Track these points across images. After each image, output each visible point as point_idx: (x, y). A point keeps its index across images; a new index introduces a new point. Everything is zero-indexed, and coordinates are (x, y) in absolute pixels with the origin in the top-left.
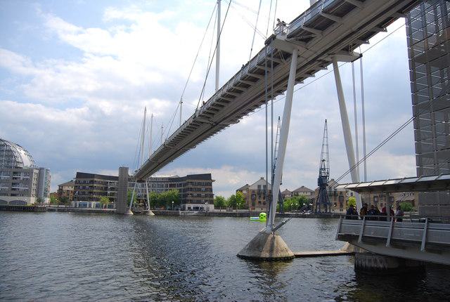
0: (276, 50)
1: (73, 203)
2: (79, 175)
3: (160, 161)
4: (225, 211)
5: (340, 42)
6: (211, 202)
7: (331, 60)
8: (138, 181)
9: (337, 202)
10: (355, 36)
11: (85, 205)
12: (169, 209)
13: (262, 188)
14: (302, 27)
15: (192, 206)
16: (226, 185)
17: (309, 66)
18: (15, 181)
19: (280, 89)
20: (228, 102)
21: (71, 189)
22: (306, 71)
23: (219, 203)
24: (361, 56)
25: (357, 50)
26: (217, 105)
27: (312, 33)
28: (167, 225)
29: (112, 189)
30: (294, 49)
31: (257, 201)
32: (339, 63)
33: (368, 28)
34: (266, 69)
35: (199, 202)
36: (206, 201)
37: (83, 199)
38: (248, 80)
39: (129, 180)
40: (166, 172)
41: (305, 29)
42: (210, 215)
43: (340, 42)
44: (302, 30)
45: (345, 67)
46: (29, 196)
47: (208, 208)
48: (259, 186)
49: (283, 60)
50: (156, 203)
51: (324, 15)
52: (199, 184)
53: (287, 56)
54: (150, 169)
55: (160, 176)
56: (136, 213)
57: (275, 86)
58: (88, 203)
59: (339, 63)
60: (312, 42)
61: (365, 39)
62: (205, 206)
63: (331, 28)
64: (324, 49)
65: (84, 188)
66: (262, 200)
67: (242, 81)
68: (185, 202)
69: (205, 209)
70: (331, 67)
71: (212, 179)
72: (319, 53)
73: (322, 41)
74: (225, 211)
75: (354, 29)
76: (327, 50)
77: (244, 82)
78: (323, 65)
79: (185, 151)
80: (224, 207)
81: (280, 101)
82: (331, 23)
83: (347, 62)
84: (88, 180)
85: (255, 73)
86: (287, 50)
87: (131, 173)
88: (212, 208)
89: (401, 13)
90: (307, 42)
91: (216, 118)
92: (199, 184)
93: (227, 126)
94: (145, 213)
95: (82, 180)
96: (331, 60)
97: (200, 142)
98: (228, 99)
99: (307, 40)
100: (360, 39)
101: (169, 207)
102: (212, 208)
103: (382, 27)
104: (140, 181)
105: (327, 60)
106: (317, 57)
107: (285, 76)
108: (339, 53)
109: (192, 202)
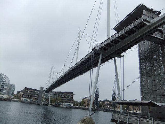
1: (22, 99)
2: (26, 88)
4: (77, 106)
6: (72, 103)
8: (47, 93)
15: (65, 104)
16: (78, 98)
21: (22, 93)
23: (75, 103)
24: (123, 56)
25: (122, 54)
32: (116, 58)
36: (70, 102)
37: (26, 98)
39: (44, 91)
42: (71, 108)
45: (118, 59)
53: (99, 54)
59: (116, 58)
60: (106, 51)
61: (124, 51)
70: (113, 59)
74: (77, 106)
77: (85, 62)
78: (111, 58)
80: (77, 105)
81: (95, 70)
88: (72, 105)
95: (26, 90)
98: (31, 97)
102: (72, 105)
103: (130, 48)
109: (65, 102)
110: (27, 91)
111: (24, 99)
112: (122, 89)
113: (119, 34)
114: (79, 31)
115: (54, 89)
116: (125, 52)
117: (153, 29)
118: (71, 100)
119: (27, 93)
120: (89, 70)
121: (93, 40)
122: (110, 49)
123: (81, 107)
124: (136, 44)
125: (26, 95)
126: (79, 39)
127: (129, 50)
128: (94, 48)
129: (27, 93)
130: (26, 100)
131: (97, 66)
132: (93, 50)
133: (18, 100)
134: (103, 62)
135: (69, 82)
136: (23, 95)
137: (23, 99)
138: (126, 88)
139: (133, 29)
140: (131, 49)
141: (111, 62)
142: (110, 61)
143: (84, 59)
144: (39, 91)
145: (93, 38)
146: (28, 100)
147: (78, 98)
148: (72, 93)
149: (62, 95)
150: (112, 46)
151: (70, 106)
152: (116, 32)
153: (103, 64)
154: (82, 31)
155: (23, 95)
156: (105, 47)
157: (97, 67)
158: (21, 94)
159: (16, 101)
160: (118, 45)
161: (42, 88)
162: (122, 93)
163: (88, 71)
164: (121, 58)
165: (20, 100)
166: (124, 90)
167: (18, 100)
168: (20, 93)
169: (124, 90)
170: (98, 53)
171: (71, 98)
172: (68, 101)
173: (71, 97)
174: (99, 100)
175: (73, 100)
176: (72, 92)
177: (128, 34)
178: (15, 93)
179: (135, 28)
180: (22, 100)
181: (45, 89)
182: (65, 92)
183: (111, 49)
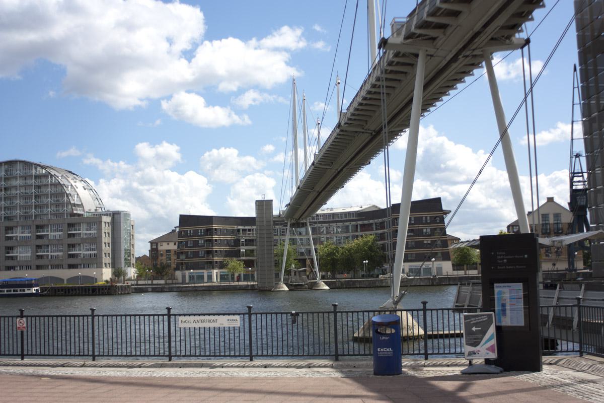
1: (178, 274)
6: (446, 257)
12: (363, 276)
13: (551, 221)
18: (40, 242)
21: (173, 247)
24: (528, 42)
37: (196, 266)
47: (440, 269)
53: (417, 56)
54: (304, 207)
56: (293, 288)
62: (434, 265)
73: (448, 44)
78: (476, 65)
81: (401, 142)
84: (202, 228)
88: (447, 267)
94: (313, 286)
95: (190, 229)
110: (196, 233)
111: (187, 273)
115: (324, 201)
116: (532, 19)
120: (382, 148)
122: (445, 35)
125: (196, 255)
129: (196, 244)
130: (201, 278)
131: (408, 126)
133: (162, 282)
134: (427, 105)
136: (183, 257)
137: (184, 277)
141: (481, 73)
142: (476, 72)
144: (254, 224)
146: (210, 277)
149: (382, 223)
151: (434, 272)
155: (183, 257)
158: (168, 251)
159: (152, 291)
163: (468, 73)
165: (170, 281)
167: (162, 282)
168: (163, 247)
171: (79, 290)
173: (434, 226)
178: (142, 249)
180: (180, 280)
181: (279, 208)
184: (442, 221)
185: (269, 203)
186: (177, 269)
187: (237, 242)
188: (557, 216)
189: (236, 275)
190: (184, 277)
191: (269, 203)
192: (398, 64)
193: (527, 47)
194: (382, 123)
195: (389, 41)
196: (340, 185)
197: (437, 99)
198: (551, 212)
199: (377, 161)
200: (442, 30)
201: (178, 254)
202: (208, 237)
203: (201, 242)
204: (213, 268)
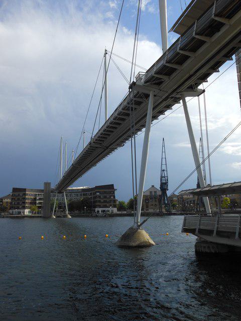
0: (138, 93)
2: (15, 190)
3: (105, 144)
4: (125, 212)
5: (183, 83)
6: (115, 206)
7: (181, 96)
8: (58, 193)
9: (157, 203)
10: (194, 78)
11: (20, 213)
12: (83, 213)
14: (153, 75)
15: (100, 210)
16: (123, 195)
17: (164, 102)
19: (168, 104)
20: (119, 124)
21: (9, 200)
22: (159, 111)
23: (121, 207)
24: (204, 91)
25: (201, 87)
26: (115, 123)
27: (161, 79)
28: (85, 223)
29: (40, 199)
30: (150, 91)
31: (150, 203)
32: (187, 99)
33: (203, 71)
34: (134, 106)
35: (106, 206)
36: (111, 205)
37: (18, 208)
38: (128, 109)
39: (52, 191)
40: (79, 185)
41: (156, 76)
42: (113, 215)
43: (183, 83)
44: (153, 77)
45: (191, 101)
46: (24, 208)
47: (112, 211)
48: (151, 192)
49: (145, 99)
50: (73, 207)
51: (167, 65)
52: (105, 192)
53: (147, 96)
54: (65, 184)
55: (75, 188)
56: (58, 217)
57: (136, 124)
58: (22, 211)
59: (187, 99)
60: (163, 85)
61: (204, 78)
62: (110, 209)
63: (174, 74)
64: (172, 90)
65: (18, 199)
66: (154, 203)
67: (119, 116)
68: (95, 207)
69: (110, 211)
70: (181, 101)
71: (115, 188)
72: (170, 92)
73: (170, 83)
74: (125, 212)
75: (192, 72)
76: (175, 90)
77: (120, 117)
78: (176, 101)
79: (89, 168)
81: (141, 135)
82: (174, 70)
83: (194, 96)
84: (21, 194)
85: (122, 115)
86: (146, 92)
87: (53, 186)
88: (115, 210)
89: (227, 57)
90: (160, 85)
91: (105, 144)
92: (105, 192)
93: (116, 148)
94: (65, 216)
95: (17, 194)
96: (181, 96)
97: (100, 160)
98: (103, 139)
99: (160, 83)
100: (158, 112)
101: (82, 212)
102: (115, 210)
103: (215, 68)
104: (60, 192)
105: (178, 96)
106: (169, 95)
107: (128, 128)
108: (186, 91)
109: (100, 207)
111: (14, 211)
112: (206, 155)
113: (186, 40)
114: (104, 52)
116: (207, 81)
117: (235, 37)
118: (113, 202)
119: (18, 199)
121: (134, 66)
123: (133, 212)
124: (228, 57)
126: (106, 69)
127: (214, 76)
128: (134, 83)
131: (144, 126)
132: (130, 87)
134: (155, 117)
135: (98, 165)
138: (213, 152)
139: (216, 21)
140: (218, 71)
141: (178, 107)
143: (117, 112)
145: (134, 62)
146: (24, 213)
147: (123, 195)
148: (111, 187)
150: (173, 70)
152: (177, 36)
153: (155, 121)
154: (109, 50)
156: (157, 78)
157: (144, 130)
160: (184, 67)
161: (47, 185)
162: (207, 162)
163: (169, 107)
164: (198, 96)
166: (209, 156)
169: (209, 156)
170: (144, 94)
172: (104, 204)
174: (169, 193)
175: (115, 201)
176: (111, 187)
177: (206, 36)
179: (221, 16)
182: (97, 187)
183: (171, 78)
184: (114, 193)
185: (49, 184)
186: (10, 209)
187: (35, 199)
188: (155, 192)
189: (34, 212)
190: (13, 212)
191: (49, 184)
192: (105, 134)
193: (203, 94)
194: (130, 125)
195: (137, 83)
196: (80, 176)
197: (108, 154)
198: (153, 190)
199: (128, 144)
200: (168, 77)
201: (11, 203)
202: (24, 197)
203: (21, 199)
204: (25, 209)
